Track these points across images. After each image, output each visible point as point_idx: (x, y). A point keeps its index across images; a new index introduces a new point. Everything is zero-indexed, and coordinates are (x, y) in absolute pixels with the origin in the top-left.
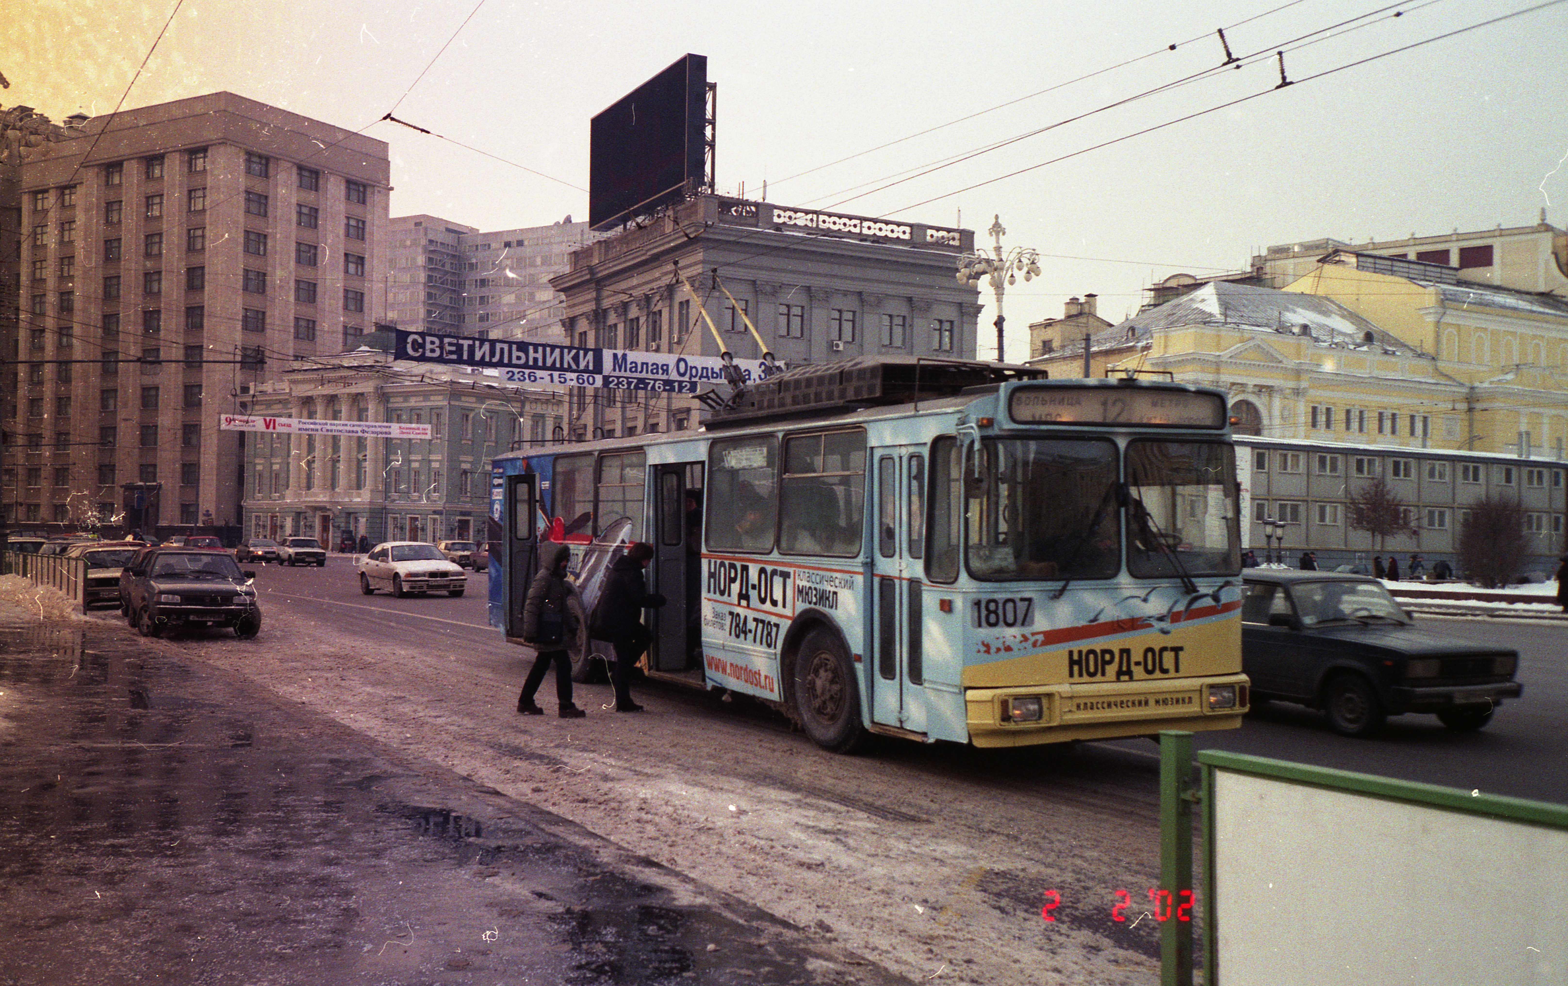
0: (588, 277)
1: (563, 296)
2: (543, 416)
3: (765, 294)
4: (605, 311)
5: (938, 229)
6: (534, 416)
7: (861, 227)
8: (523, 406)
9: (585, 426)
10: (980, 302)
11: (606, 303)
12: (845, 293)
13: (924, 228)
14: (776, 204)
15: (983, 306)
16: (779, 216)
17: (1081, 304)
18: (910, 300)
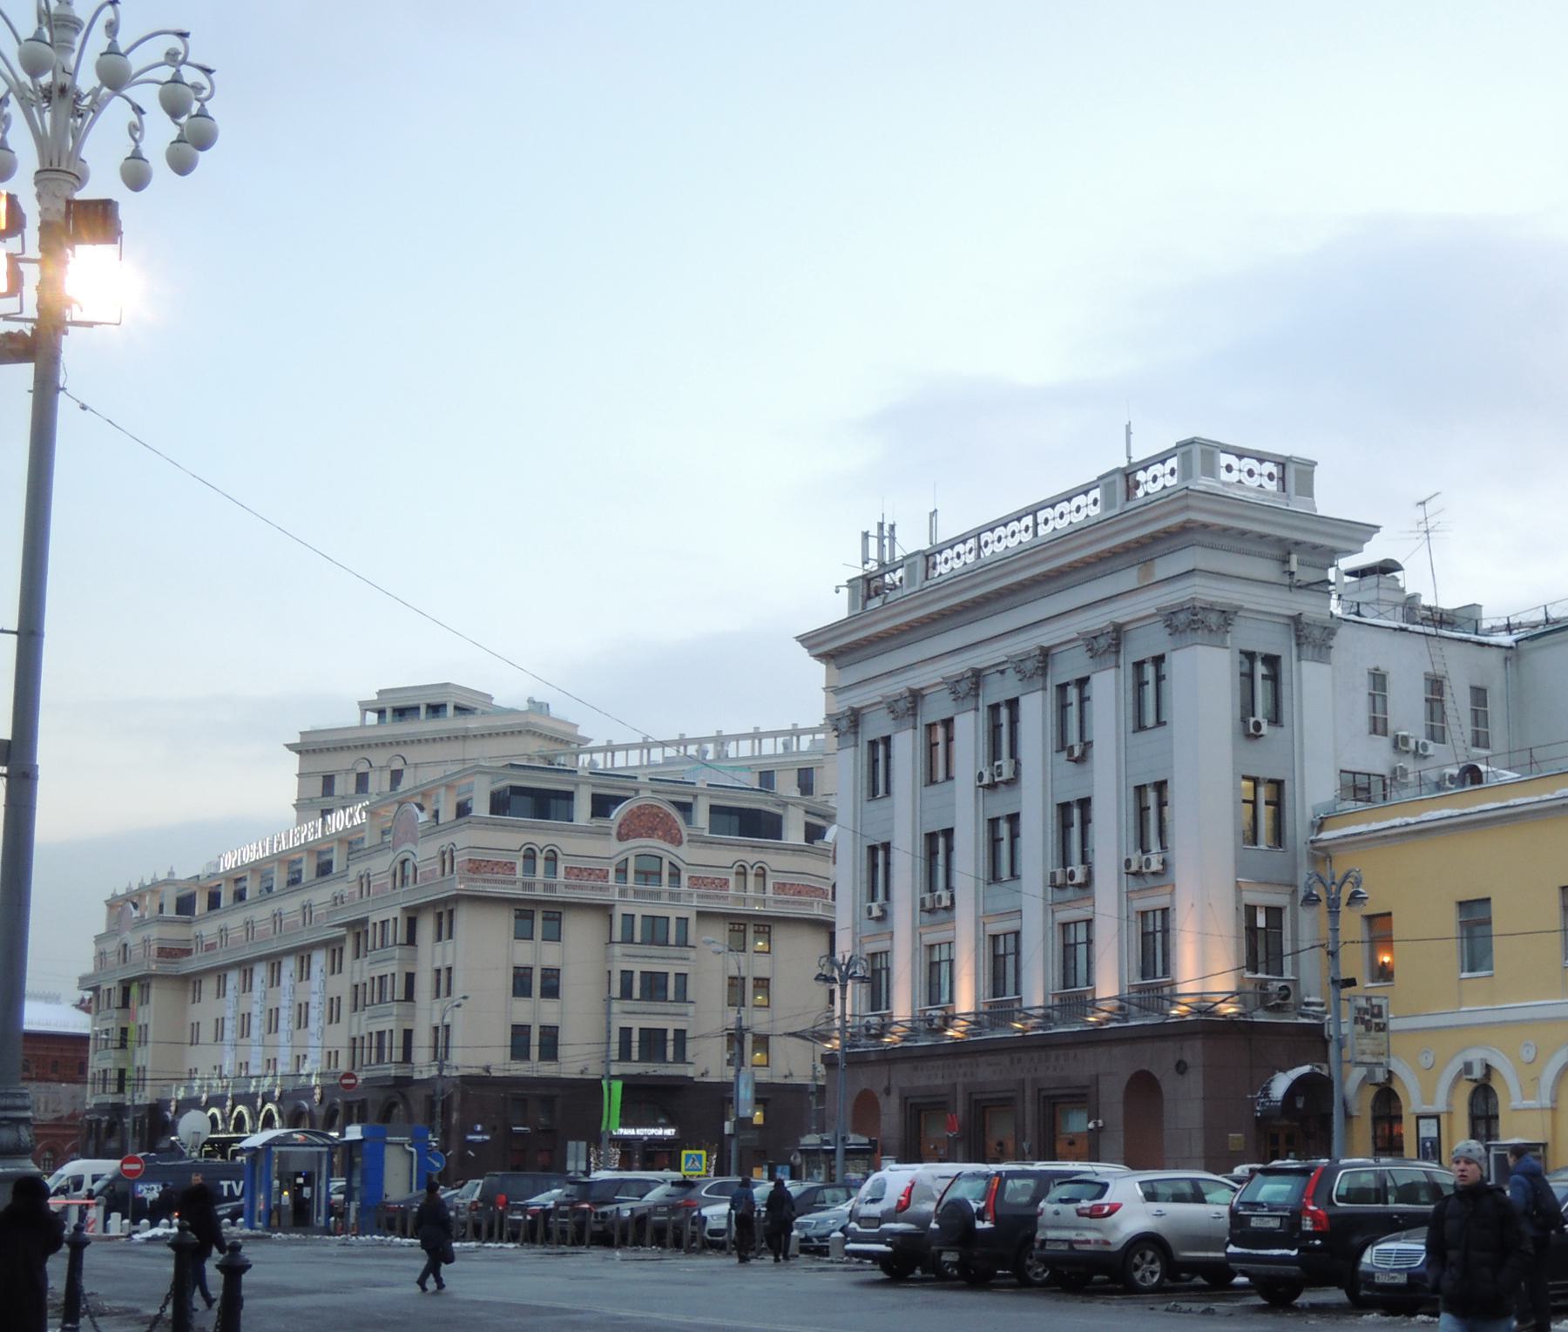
16: (1229, 468)
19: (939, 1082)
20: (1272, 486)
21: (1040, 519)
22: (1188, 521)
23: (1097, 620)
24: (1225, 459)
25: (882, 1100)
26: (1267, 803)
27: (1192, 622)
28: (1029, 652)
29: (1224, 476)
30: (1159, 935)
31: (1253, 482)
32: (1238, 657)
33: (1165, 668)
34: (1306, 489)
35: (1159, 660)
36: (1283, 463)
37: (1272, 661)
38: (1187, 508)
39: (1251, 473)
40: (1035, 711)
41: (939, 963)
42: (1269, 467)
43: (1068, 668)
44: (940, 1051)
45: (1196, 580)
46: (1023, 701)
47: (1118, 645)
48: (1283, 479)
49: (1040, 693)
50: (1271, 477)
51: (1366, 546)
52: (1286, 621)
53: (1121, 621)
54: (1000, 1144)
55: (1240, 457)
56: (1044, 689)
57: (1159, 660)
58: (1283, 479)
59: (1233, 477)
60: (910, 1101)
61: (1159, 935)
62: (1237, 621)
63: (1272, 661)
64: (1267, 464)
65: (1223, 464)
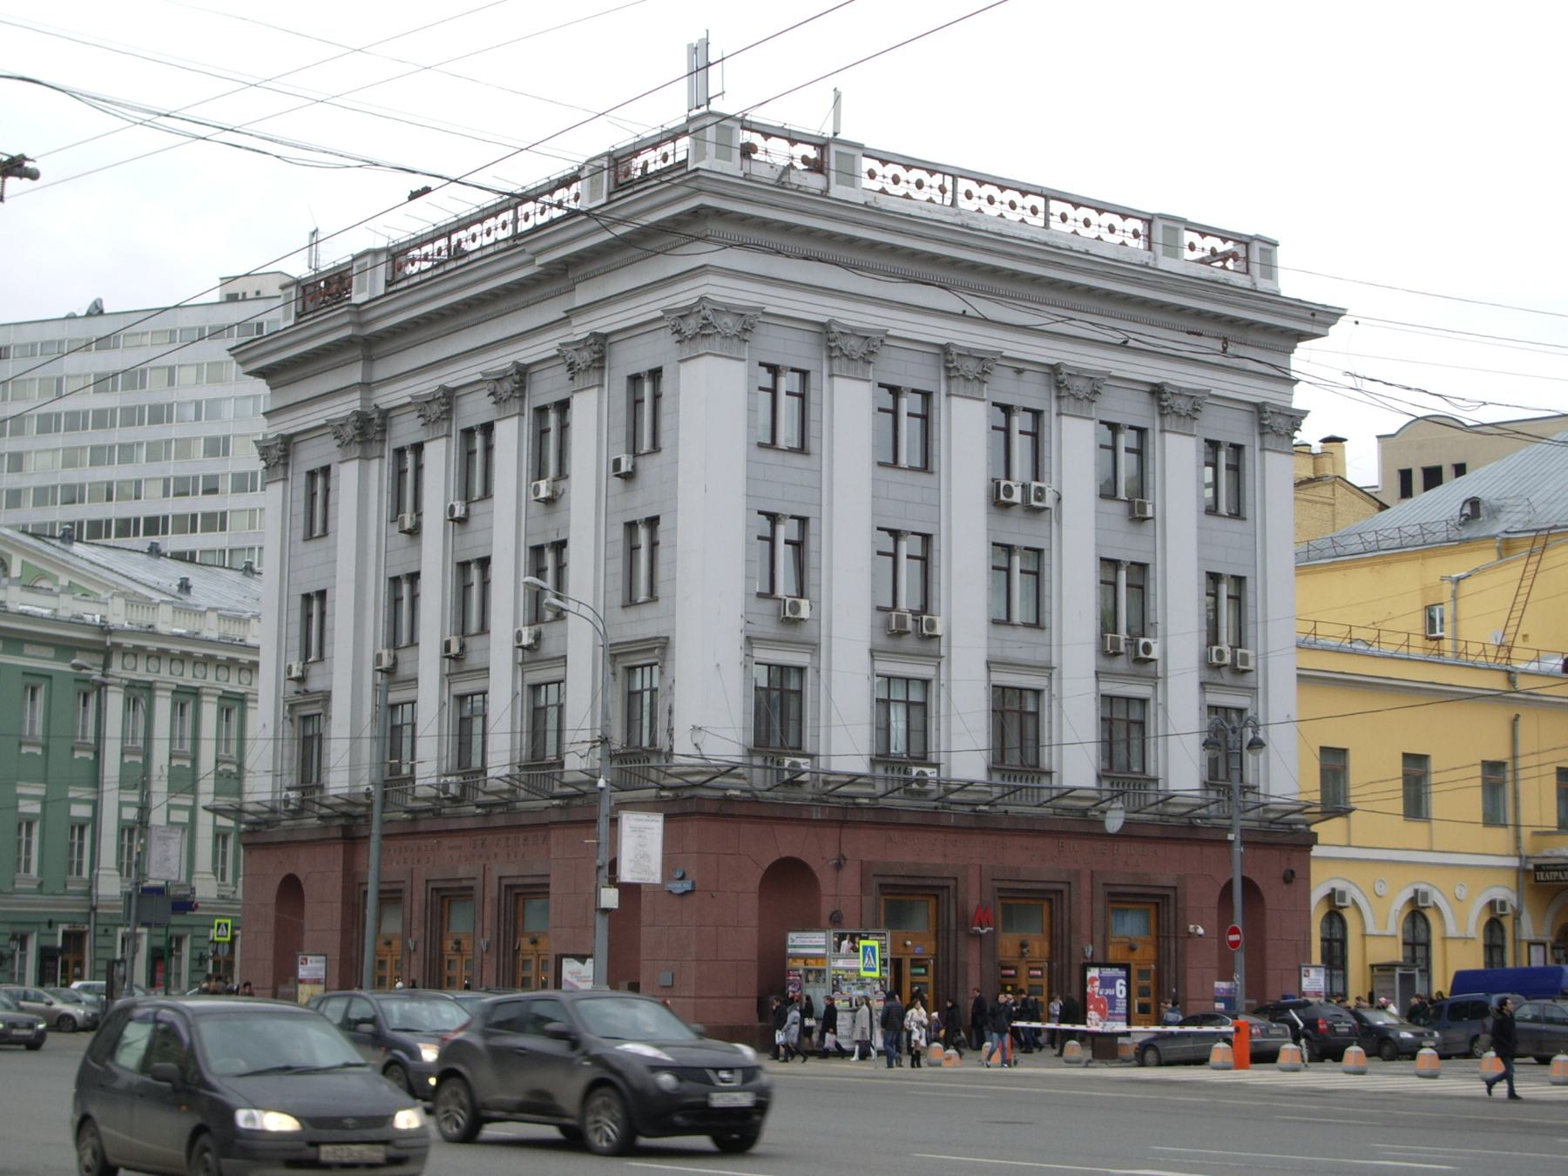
0: (347, 332)
1: (261, 386)
2: (149, 687)
3: (849, 358)
4: (386, 414)
5: (1204, 232)
6: (131, 686)
7: (1047, 214)
8: (106, 665)
9: (326, 697)
10: (1297, 404)
11: (388, 397)
12: (1020, 368)
13: (1176, 224)
14: (869, 144)
15: (1304, 414)
16: (872, 175)
17: (1315, 456)
18: (1157, 391)
19: (939, 860)
20: (1139, 244)
21: (510, 227)
22: (702, 207)
23: (501, 361)
24: (867, 164)
25: (825, 878)
26: (787, 542)
27: (699, 328)
28: (505, 371)
29: (867, 183)
30: (647, 695)
31: (1013, 216)
32: (1203, 444)
33: (666, 387)
34: (1269, 269)
35: (656, 374)
36: (1149, 221)
37: (1237, 449)
38: (699, 191)
39: (1013, 205)
40: (510, 438)
41: (401, 726)
42: (1139, 225)
43: (546, 389)
44: (304, 837)
45: (711, 279)
46: (498, 427)
47: (602, 359)
48: (1149, 237)
49: (280, 485)
50: (1136, 234)
51: (1332, 329)
52: (1147, 389)
53: (605, 330)
54: (458, 943)
55: (1203, 235)
56: (448, 436)
57: (656, 374)
58: (1149, 237)
59: (875, 185)
60: (505, 882)
61: (647, 695)
62: (761, 329)
63: (1237, 449)
64: (1106, 215)
65: (1187, 243)
